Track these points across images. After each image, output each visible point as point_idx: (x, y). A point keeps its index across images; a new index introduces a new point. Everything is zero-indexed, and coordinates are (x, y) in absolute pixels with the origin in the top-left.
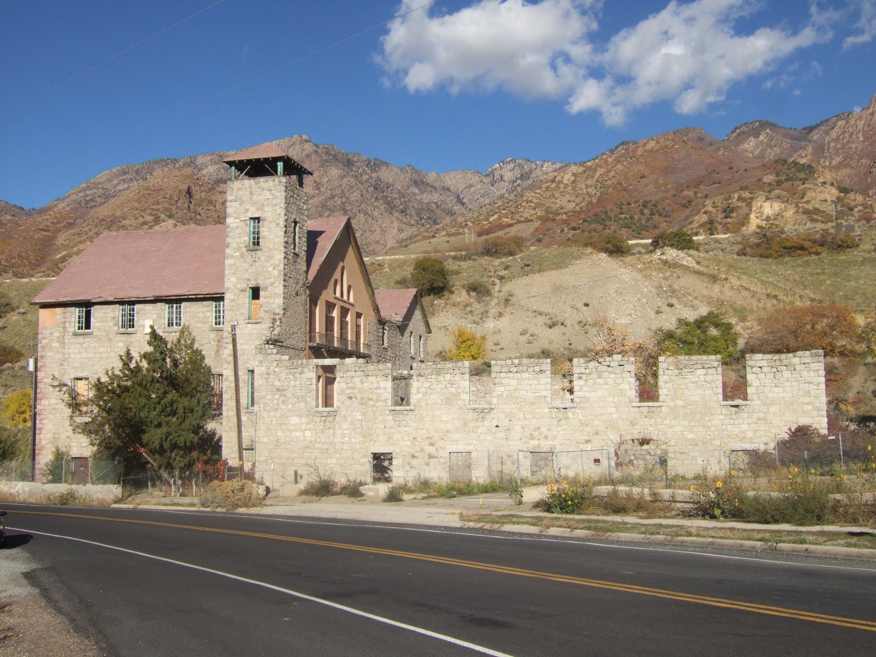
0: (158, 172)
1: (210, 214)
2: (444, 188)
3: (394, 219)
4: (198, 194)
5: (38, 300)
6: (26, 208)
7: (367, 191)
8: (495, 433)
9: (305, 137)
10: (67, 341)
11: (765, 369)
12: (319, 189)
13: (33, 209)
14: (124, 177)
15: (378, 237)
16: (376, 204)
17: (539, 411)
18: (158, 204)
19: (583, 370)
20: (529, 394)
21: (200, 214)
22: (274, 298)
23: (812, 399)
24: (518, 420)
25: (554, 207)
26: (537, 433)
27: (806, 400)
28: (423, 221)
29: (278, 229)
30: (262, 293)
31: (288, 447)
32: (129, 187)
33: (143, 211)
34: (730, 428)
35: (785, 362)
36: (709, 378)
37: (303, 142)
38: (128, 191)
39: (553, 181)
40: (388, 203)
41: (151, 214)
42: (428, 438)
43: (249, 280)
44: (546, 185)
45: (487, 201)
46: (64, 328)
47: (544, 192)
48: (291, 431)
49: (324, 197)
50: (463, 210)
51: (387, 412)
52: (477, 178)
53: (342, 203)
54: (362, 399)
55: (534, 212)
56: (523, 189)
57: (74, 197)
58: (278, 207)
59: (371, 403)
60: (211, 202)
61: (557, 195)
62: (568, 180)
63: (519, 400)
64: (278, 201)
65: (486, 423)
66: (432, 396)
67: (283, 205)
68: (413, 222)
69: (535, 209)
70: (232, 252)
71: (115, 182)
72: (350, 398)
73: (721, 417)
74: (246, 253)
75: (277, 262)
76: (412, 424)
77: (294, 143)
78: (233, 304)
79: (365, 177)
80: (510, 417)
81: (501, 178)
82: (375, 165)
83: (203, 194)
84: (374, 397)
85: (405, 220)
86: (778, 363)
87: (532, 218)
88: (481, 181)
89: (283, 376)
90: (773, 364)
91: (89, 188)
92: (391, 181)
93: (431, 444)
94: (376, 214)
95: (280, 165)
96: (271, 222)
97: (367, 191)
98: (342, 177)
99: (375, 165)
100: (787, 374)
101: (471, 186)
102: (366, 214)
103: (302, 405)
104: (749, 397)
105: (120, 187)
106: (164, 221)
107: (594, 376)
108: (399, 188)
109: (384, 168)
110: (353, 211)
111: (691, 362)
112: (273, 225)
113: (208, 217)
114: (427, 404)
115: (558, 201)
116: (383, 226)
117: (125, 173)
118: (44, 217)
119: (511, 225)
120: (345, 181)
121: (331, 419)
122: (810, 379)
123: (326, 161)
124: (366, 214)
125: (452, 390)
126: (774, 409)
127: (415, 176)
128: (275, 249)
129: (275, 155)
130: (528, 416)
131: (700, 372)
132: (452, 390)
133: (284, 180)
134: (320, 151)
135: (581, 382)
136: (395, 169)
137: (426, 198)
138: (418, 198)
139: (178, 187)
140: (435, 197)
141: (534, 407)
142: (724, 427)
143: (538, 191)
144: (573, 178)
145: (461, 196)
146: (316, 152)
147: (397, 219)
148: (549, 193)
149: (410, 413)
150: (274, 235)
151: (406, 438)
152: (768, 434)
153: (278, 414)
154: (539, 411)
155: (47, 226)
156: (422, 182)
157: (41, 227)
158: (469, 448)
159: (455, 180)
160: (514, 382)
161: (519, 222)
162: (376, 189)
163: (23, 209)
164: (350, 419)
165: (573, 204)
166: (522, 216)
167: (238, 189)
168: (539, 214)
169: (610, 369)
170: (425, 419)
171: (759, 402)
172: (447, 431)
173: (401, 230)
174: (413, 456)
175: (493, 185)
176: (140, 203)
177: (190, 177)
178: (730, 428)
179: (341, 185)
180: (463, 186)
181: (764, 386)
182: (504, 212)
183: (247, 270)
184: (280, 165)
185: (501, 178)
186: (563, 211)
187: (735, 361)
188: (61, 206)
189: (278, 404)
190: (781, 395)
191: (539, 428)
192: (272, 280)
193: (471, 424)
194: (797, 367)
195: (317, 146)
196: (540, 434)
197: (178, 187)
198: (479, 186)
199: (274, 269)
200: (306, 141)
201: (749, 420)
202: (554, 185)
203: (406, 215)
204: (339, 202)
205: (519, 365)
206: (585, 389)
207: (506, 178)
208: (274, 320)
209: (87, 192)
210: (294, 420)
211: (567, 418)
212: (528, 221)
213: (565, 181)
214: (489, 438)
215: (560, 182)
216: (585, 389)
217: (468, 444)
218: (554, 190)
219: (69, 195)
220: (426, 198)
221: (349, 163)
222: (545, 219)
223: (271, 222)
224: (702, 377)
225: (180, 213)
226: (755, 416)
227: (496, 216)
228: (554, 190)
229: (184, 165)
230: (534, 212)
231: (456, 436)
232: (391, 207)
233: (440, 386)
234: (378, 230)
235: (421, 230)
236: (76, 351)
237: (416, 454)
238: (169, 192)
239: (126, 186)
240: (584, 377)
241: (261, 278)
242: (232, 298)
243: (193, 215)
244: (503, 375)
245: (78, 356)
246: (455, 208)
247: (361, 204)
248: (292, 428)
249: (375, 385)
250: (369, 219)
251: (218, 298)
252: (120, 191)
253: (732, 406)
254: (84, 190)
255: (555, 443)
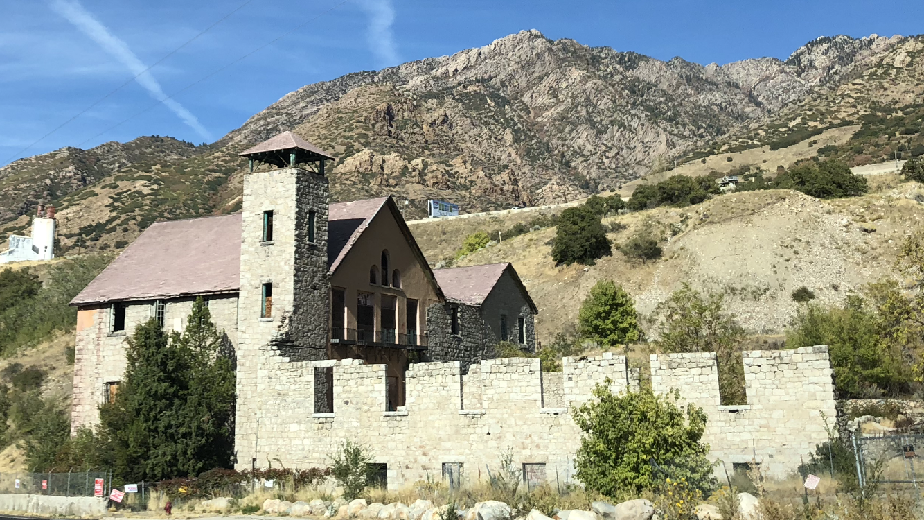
0: (353, 91)
1: (415, 138)
2: (729, 84)
3: (660, 130)
4: (401, 115)
5: (76, 300)
6: (196, 144)
7: (621, 96)
8: (486, 442)
9: (534, 31)
10: (101, 343)
11: (764, 368)
12: (556, 97)
13: (205, 145)
14: (313, 98)
15: (640, 156)
16: (633, 112)
17: (530, 416)
18: (352, 130)
19: (572, 371)
20: (520, 397)
21: (402, 140)
22: (284, 298)
23: (818, 403)
24: (510, 426)
25: (885, 101)
26: (528, 441)
27: (812, 404)
28: (702, 130)
29: (290, 222)
30: (273, 290)
31: (288, 456)
32: (318, 110)
33: (332, 140)
34: (730, 436)
35: (786, 360)
36: (703, 378)
37: (533, 38)
38: (316, 117)
39: (879, 65)
40: (648, 108)
41: (343, 144)
42: (421, 447)
43: (262, 276)
44: (868, 72)
45: (793, 97)
46: (100, 329)
47: (868, 81)
48: (290, 439)
49: (563, 107)
50: (759, 112)
51: (382, 418)
52: (776, 68)
53: (588, 113)
54: (357, 404)
55: (853, 110)
56: (841, 78)
57: (252, 127)
58: (290, 199)
59: (366, 408)
60: (416, 123)
61: (886, 85)
62: (902, 62)
63: (510, 404)
64: (290, 192)
65: (478, 430)
66: (424, 400)
67: (295, 198)
68: (687, 133)
69: (854, 106)
70: (247, 247)
71: (302, 104)
72: (347, 402)
73: (720, 424)
74: (261, 248)
75: (288, 257)
76: (406, 431)
77: (521, 40)
78: (247, 302)
79: (617, 77)
80: (501, 423)
81: (811, 64)
82: (630, 61)
83: (405, 114)
84: (369, 401)
85: (676, 131)
86: (778, 361)
87: (851, 118)
88: (782, 71)
89: (284, 379)
90: (773, 362)
91: (270, 115)
92: (653, 79)
93: (424, 454)
94: (634, 124)
95: (292, 157)
96: (283, 215)
97: (621, 96)
98: (584, 80)
99: (630, 61)
100: (789, 373)
101: (768, 78)
102: (622, 125)
103: (301, 411)
104: (748, 400)
105: (308, 111)
106: (358, 151)
107: (584, 377)
108: (665, 88)
109: (643, 63)
110: (604, 123)
111: (683, 361)
112: (285, 218)
113: (413, 143)
114: (420, 409)
115: (888, 92)
116: (646, 140)
117: (313, 93)
118: (216, 155)
119: (819, 132)
120: (590, 84)
121: (328, 426)
122: (815, 380)
123: (564, 60)
124: (622, 125)
125: (444, 393)
126: (776, 414)
127: (686, 71)
128: (286, 243)
129: (287, 147)
130: (519, 422)
131: (696, 371)
132: (444, 393)
133: (295, 171)
134: (554, 48)
135: (571, 384)
136: (658, 64)
137: (703, 99)
138: (692, 99)
139: (374, 108)
140: (718, 97)
141: (524, 412)
142: (723, 436)
143: (858, 81)
144: (908, 59)
145: (755, 93)
146: (550, 50)
147: (665, 130)
148: (875, 83)
149: (404, 418)
150: (286, 228)
151: (400, 446)
152: (773, 444)
153: (279, 421)
154: (530, 416)
155: (218, 165)
156: (698, 78)
157: (211, 168)
158: (461, 459)
159: (744, 72)
160: (504, 384)
161: (832, 126)
162: (633, 92)
163: (191, 145)
164: (346, 426)
165: (913, 95)
166: (836, 118)
167: (254, 183)
168: (862, 112)
169: (600, 368)
170: (419, 426)
171: (760, 407)
172: (440, 439)
173: (671, 145)
174: (407, 468)
175: (799, 75)
176: (329, 130)
177: (390, 93)
178: (730, 436)
179: (585, 90)
180: (756, 79)
181: (765, 388)
182: (810, 113)
183: (260, 265)
184: (292, 157)
185: (811, 64)
186: (897, 106)
187: (29, 416)
188: (239, 138)
189: (279, 410)
190: (784, 398)
191: (530, 436)
192: (283, 276)
193: (464, 431)
194: (799, 365)
195: (551, 42)
196: (532, 442)
197: (374, 108)
198: (779, 78)
199: (285, 264)
200: (537, 36)
201: (750, 428)
202: (880, 71)
203: (676, 124)
204: (584, 112)
205: (508, 364)
206: (575, 391)
207: (817, 64)
208: (284, 318)
209: (268, 120)
210: (294, 427)
211: (559, 425)
212: (846, 123)
213: (897, 64)
214: (481, 446)
215: (890, 66)
216: (575, 391)
217: (462, 454)
218: (882, 77)
219: (246, 125)
220: (703, 99)
221: (594, 61)
222: (866, 120)
223: (283, 215)
224: (697, 378)
225: (378, 140)
226: (757, 422)
227: (798, 120)
228: (882, 77)
229: (384, 78)
230: (853, 110)
231: (448, 445)
232: (654, 115)
233: (432, 389)
234: (639, 145)
235: (699, 143)
236: (110, 353)
237: (410, 466)
238: (365, 114)
239: (315, 109)
240: (574, 377)
241: (274, 274)
242: (246, 295)
243: (394, 141)
244: (493, 376)
245: (112, 358)
246: (747, 110)
247: (614, 113)
248: (291, 435)
249: (370, 388)
250: (626, 132)
251: (235, 294)
252: (307, 115)
253: (731, 411)
254: (264, 117)
255: (547, 453)
